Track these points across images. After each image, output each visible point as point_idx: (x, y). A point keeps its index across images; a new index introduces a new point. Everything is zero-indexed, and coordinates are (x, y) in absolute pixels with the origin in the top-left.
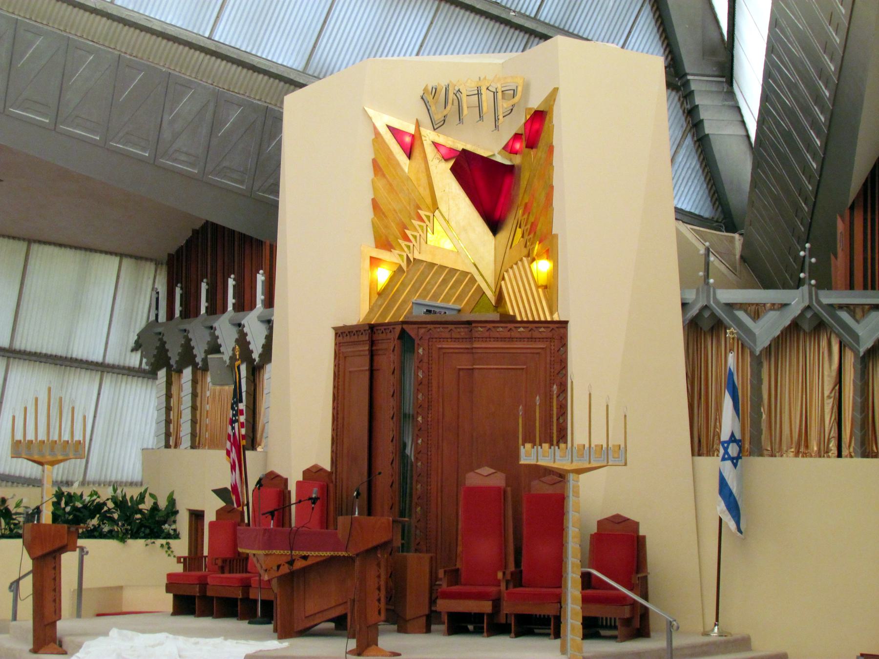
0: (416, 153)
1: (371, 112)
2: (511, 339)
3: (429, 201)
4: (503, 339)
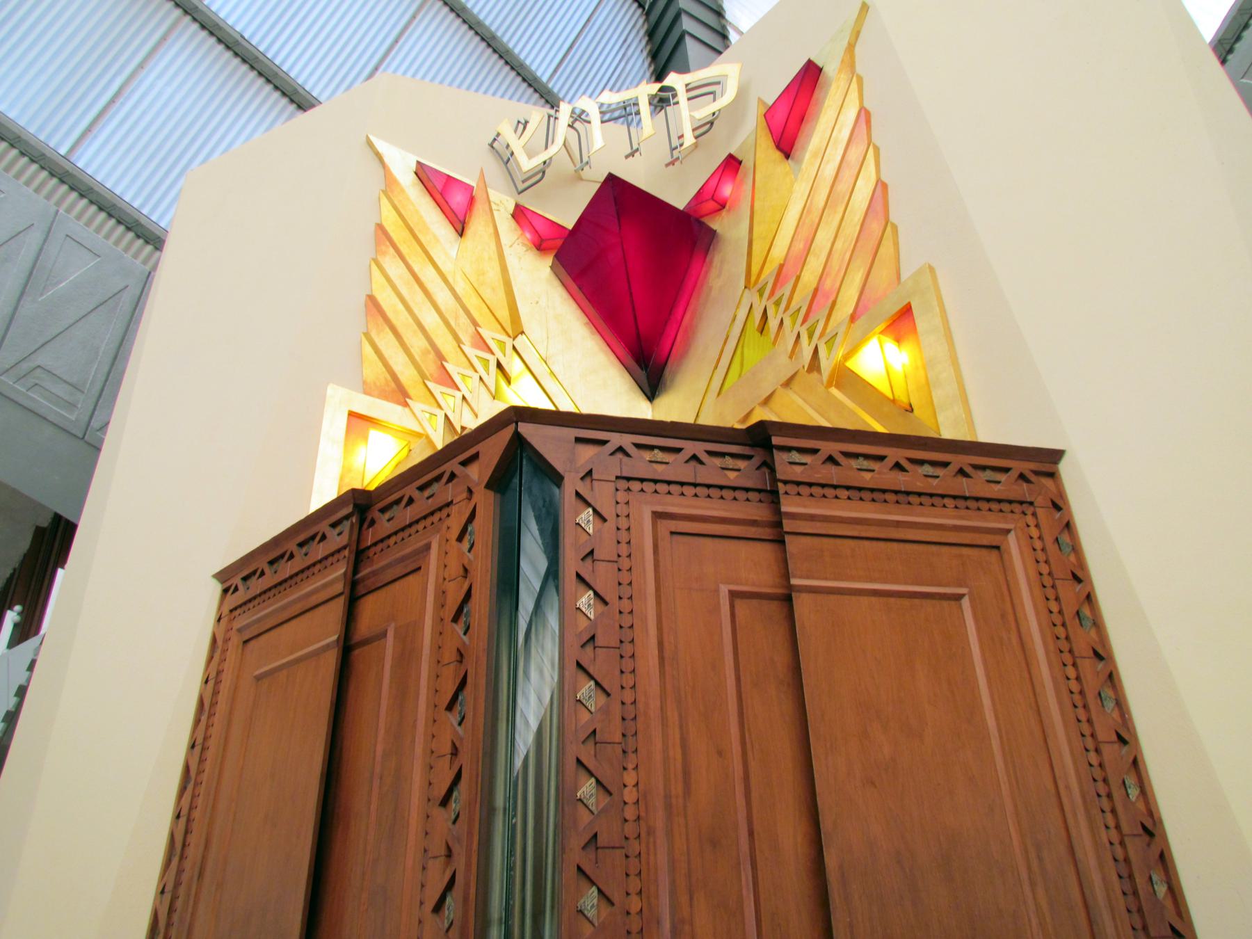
0: (478, 225)
1: (381, 146)
2: (903, 495)
3: (504, 314)
4: (876, 493)
